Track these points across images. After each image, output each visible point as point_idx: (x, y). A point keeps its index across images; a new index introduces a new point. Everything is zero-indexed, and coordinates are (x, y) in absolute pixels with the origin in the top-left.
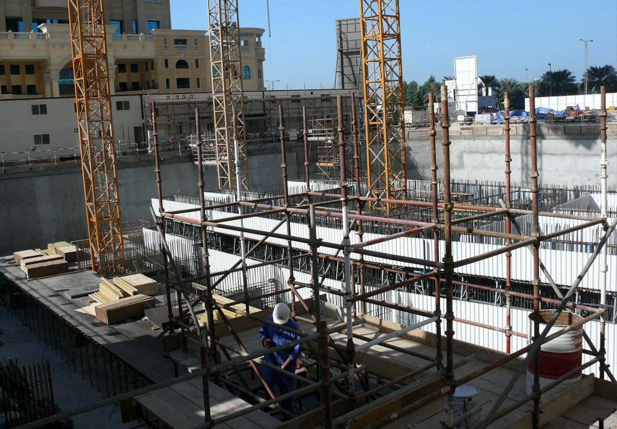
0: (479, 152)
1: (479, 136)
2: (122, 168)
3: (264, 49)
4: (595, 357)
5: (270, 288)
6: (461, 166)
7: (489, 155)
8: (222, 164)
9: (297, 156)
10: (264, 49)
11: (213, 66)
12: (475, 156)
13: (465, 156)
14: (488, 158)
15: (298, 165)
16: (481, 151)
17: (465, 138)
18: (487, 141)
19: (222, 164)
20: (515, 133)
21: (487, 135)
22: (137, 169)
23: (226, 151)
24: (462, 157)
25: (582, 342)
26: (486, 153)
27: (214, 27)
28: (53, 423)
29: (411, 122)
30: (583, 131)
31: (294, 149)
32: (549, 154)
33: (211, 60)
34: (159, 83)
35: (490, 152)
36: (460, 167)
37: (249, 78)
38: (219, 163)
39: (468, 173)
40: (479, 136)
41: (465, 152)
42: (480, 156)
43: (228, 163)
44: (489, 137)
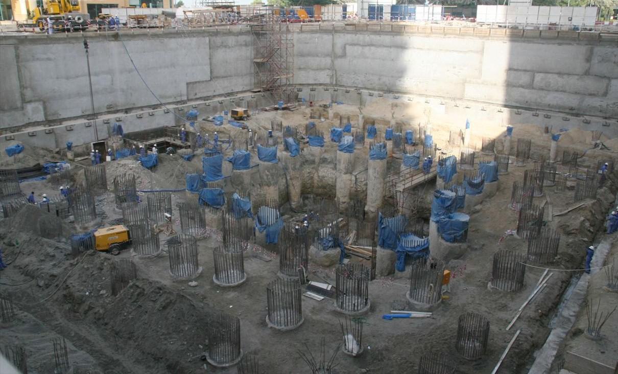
4: (445, 274)
5: (511, 305)
9: (210, 41)
12: (356, 48)
13: (348, 47)
14: (367, 49)
15: (210, 48)
16: (361, 43)
17: (348, 32)
18: (366, 36)
21: (367, 30)
25: (242, 107)
26: (366, 46)
34: (538, 360)
35: (369, 45)
37: (332, 140)
39: (350, 62)
40: (359, 31)
41: (347, 44)
42: (360, 48)
44: (369, 33)
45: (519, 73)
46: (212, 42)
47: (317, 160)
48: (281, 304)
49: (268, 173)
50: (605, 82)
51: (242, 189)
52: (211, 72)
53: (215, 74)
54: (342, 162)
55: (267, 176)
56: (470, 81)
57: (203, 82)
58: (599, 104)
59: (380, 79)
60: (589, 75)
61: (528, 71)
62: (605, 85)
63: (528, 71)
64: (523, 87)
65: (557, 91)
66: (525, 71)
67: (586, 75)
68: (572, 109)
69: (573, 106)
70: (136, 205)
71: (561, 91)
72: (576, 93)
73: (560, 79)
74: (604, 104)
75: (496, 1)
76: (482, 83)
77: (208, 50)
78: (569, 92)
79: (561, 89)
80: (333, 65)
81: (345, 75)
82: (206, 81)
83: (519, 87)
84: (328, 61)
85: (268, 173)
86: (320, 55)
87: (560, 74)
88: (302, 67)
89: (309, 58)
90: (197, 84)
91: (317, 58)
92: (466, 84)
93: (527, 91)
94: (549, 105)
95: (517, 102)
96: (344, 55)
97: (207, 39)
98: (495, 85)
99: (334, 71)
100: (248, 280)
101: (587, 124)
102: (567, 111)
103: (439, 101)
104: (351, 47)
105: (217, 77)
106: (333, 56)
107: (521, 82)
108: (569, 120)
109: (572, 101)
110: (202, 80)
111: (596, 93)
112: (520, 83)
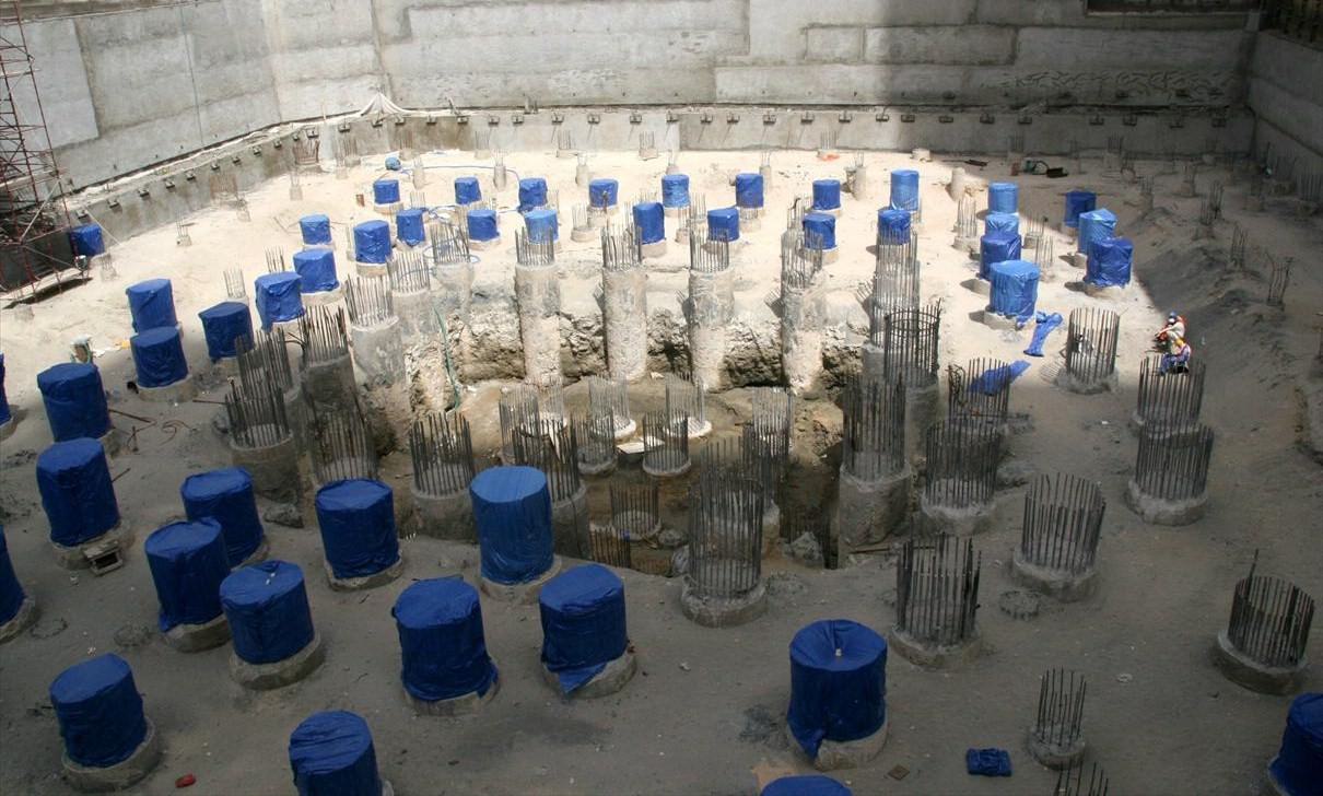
12: (434, 13)
13: (414, 16)
39: (423, 49)
42: (447, 14)
45: (832, 33)
46: (84, 33)
47: (464, 296)
48: (729, 525)
49: (381, 353)
50: (1008, 34)
51: (340, 408)
52: (98, 116)
53: (108, 119)
54: (535, 290)
55: (382, 360)
56: (725, 61)
57: (81, 144)
58: (1003, 79)
59: (506, 82)
60: (977, 23)
61: (852, 26)
62: (1009, 40)
63: (852, 26)
64: (843, 61)
65: (915, 63)
66: (845, 26)
67: (970, 23)
68: (949, 97)
69: (952, 89)
70: (721, 268)
71: (925, 62)
72: (955, 63)
73: (921, 38)
74: (1011, 81)
75: (1259, 2)
76: (754, 64)
77: (77, 56)
78: (941, 64)
79: (923, 58)
80: (380, 62)
81: (415, 83)
82: (88, 141)
83: (835, 62)
84: (367, 52)
85: (381, 353)
86: (344, 41)
87: (918, 26)
88: (305, 76)
89: (320, 51)
90: (69, 153)
91: (340, 50)
92: (717, 69)
93: (853, 69)
94: (903, 94)
95: (833, 96)
96: (406, 35)
97: (70, 24)
98: (783, 63)
99: (386, 77)
100: (695, 465)
101: (987, 126)
102: (941, 102)
103: (663, 114)
104: (422, 12)
105: (114, 128)
106: (376, 38)
107: (839, 52)
108: (952, 121)
109: (950, 80)
110: (79, 139)
111: (993, 59)
112: (837, 55)
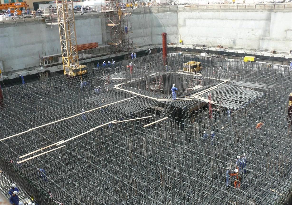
0: (194, 19)
1: (193, 10)
2: (6, 27)
3: (288, 58)
6: (184, 25)
7: (199, 20)
8: (61, 24)
10: (288, 58)
11: (61, 42)
13: (187, 20)
15: (102, 25)
19: (61, 24)
20: (212, 9)
21: (198, 9)
22: (14, 27)
23: (62, 17)
24: (185, 21)
27: (33, 87)
28: (12, 202)
29: (159, 3)
30: (247, 8)
31: (99, 17)
32: (229, 19)
33: (60, 38)
35: (199, 18)
36: (184, 26)
38: (59, 23)
40: (193, 10)
41: (187, 18)
43: (64, 23)
